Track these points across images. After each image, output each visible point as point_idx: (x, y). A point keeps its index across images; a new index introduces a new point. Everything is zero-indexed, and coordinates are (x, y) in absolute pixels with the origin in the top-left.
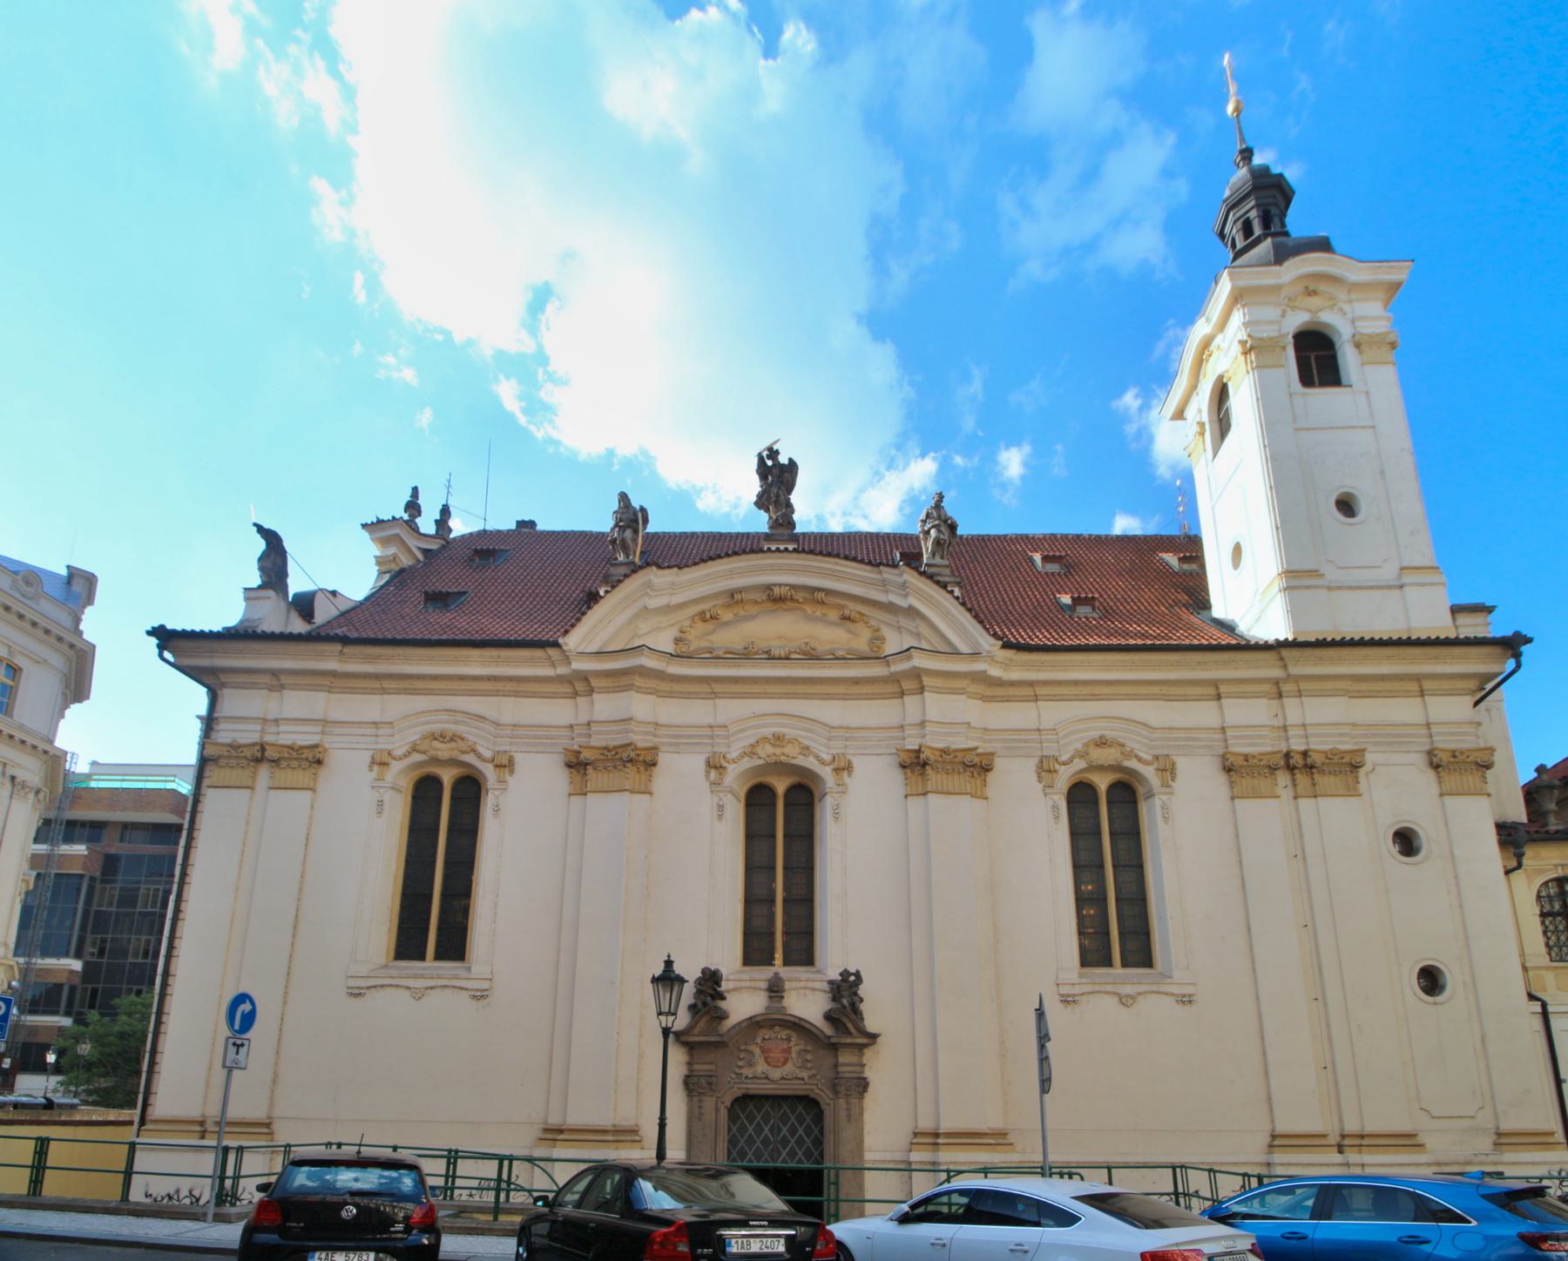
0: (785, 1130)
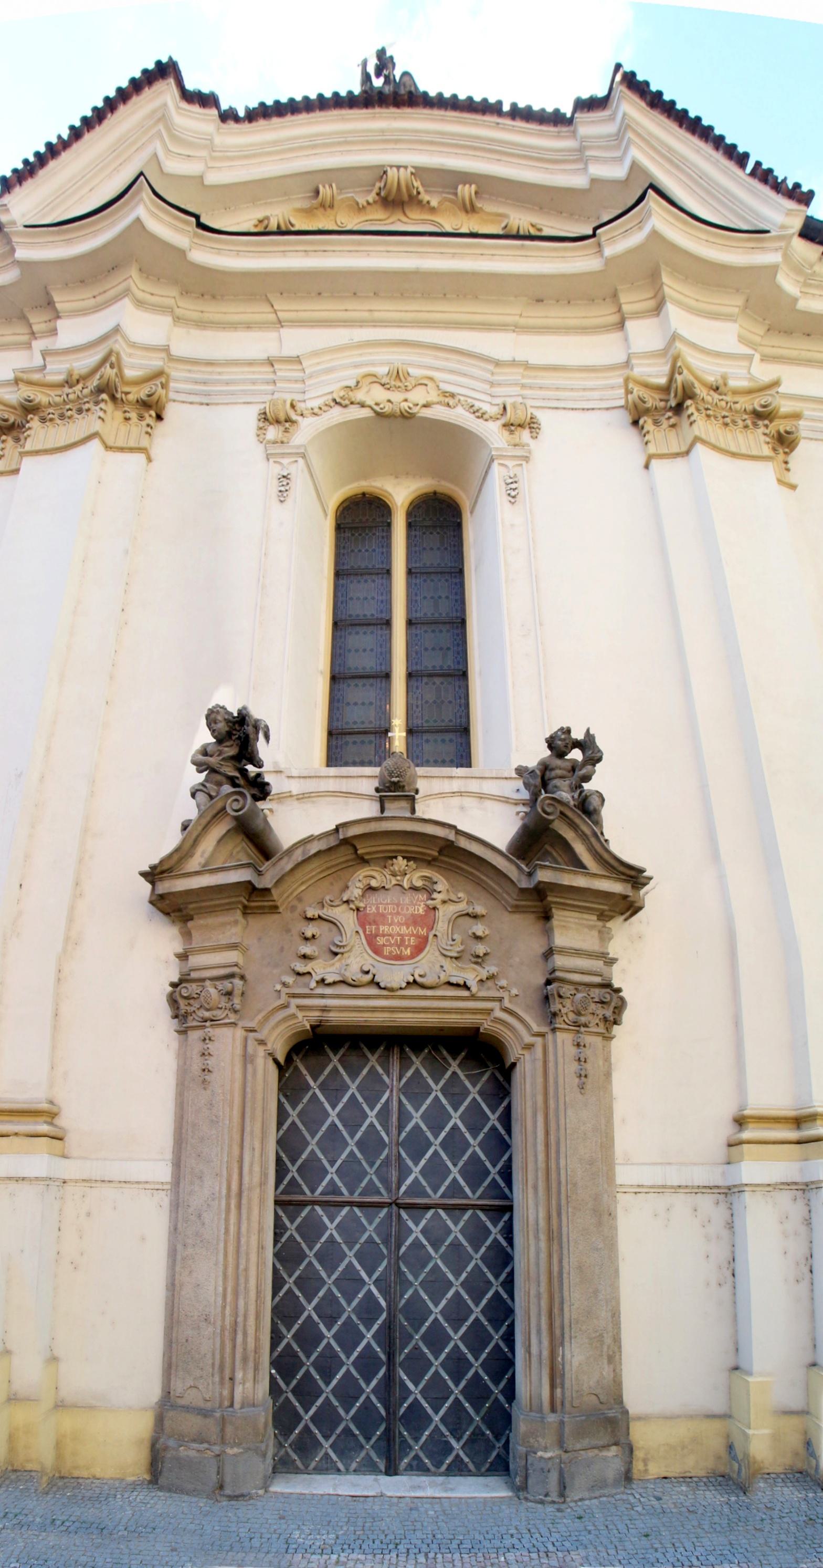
0: (416, 1118)
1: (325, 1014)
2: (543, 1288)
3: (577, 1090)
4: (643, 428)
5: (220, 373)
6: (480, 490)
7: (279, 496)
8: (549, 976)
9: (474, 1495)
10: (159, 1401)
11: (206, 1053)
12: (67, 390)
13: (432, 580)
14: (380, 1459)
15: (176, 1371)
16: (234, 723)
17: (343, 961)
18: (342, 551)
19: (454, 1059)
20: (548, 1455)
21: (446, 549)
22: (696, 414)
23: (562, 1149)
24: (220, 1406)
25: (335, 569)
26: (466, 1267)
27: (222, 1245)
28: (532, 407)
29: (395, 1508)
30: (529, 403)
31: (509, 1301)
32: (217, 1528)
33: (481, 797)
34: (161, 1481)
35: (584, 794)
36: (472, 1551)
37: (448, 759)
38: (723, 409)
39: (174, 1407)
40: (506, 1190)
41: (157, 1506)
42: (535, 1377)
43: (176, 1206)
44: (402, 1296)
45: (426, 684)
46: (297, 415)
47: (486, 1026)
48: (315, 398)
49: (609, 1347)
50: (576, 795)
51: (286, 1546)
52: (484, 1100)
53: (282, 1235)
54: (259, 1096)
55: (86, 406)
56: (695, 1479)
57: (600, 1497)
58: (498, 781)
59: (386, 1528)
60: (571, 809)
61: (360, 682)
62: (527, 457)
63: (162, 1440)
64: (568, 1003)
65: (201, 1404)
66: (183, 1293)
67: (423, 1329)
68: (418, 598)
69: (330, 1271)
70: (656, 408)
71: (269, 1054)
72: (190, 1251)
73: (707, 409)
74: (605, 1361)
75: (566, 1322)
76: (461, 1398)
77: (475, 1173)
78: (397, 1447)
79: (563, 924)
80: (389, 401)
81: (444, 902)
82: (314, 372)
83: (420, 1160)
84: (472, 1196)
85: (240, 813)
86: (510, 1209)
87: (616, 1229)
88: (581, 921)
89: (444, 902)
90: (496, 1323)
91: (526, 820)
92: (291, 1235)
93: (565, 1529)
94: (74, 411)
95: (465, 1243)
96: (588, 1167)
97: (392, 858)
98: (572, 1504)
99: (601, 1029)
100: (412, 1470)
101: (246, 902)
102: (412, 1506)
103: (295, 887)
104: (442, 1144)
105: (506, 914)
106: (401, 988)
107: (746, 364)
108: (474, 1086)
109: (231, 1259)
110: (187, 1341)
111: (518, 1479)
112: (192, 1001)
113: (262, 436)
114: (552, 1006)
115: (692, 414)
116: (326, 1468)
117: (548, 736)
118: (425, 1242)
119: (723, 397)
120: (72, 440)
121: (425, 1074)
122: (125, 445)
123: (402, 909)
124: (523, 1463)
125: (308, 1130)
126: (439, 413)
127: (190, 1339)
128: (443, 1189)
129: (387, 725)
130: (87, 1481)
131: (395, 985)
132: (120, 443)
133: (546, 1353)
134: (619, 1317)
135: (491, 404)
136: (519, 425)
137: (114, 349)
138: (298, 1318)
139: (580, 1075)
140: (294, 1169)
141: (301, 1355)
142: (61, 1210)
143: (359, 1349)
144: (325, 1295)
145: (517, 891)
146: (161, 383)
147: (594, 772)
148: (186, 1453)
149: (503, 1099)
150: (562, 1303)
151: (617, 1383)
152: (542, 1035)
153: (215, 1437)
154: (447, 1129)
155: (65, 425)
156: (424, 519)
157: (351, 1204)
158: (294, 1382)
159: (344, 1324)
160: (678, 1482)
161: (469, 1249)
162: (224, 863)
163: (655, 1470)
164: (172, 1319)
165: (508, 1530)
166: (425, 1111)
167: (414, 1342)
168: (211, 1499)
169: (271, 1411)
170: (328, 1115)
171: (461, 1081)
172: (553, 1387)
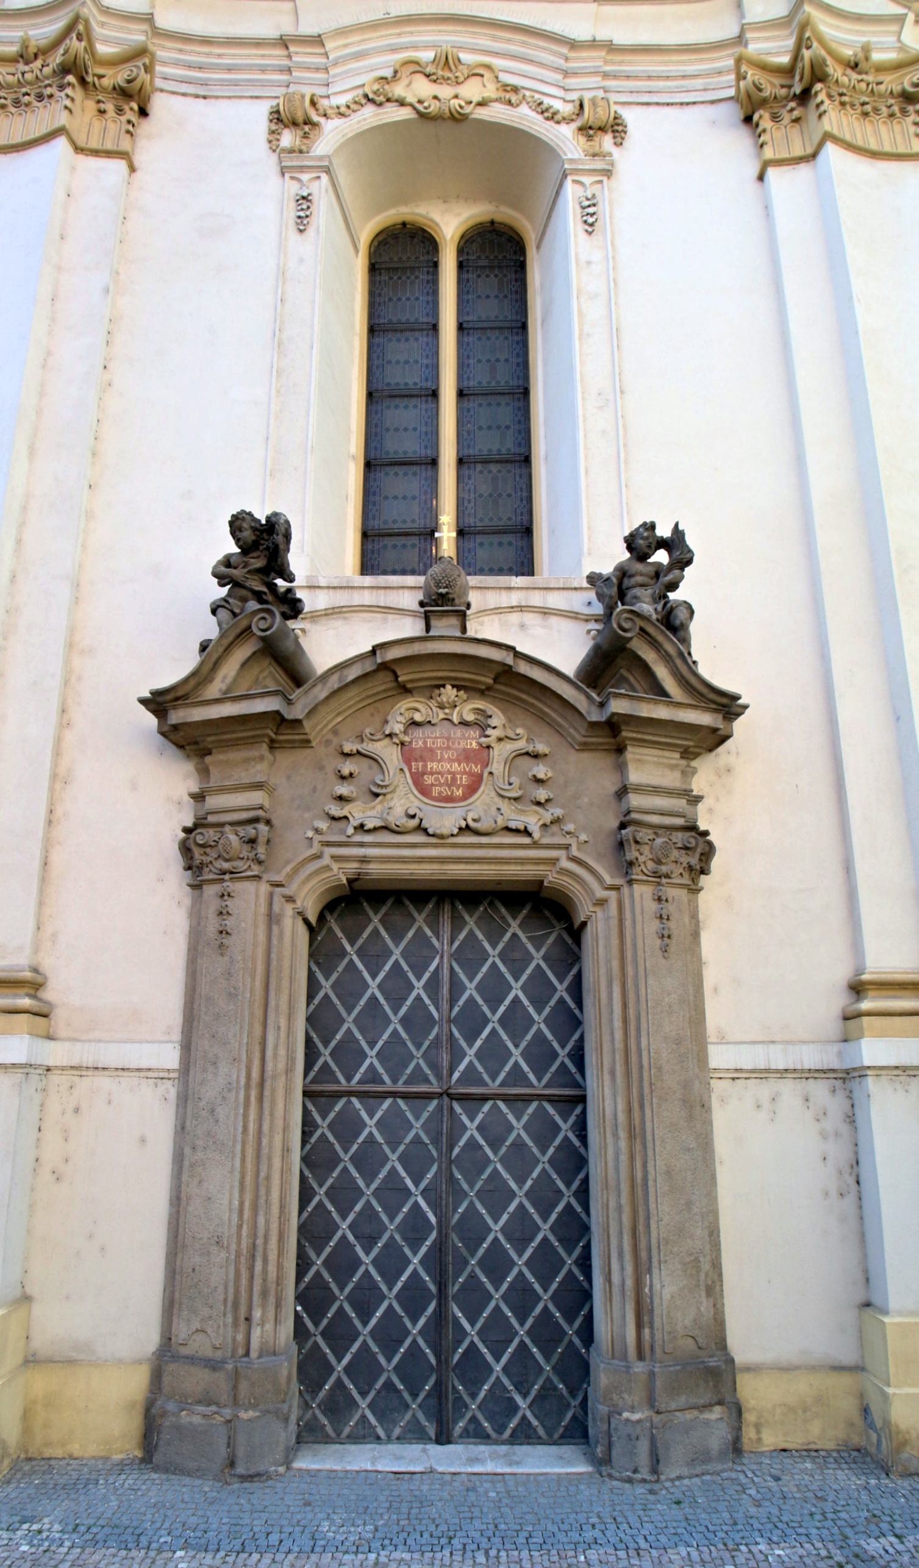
0: (471, 989)
1: (364, 866)
2: (625, 1200)
3: (659, 953)
4: (757, 125)
5: (220, 56)
6: (549, 217)
7: (297, 224)
8: (622, 819)
9: (544, 1470)
10: (158, 1350)
11: (224, 912)
12: (22, 67)
13: (489, 339)
14: (429, 1421)
15: (180, 1310)
16: (262, 532)
17: (385, 804)
18: (377, 299)
19: (514, 918)
20: (636, 1417)
21: (506, 297)
22: (827, 102)
23: (644, 1026)
24: (233, 1356)
25: (369, 323)
26: (532, 1172)
27: (239, 1147)
28: (616, 103)
29: (448, 1488)
30: (613, 97)
31: (583, 1216)
32: (225, 1521)
33: (546, 612)
34: (158, 1458)
35: (669, 605)
36: (544, 1546)
37: (505, 568)
38: (862, 93)
39: (176, 1358)
40: (578, 1077)
41: (150, 1494)
42: (617, 1314)
43: (183, 1099)
44: (455, 1210)
45: (481, 472)
46: (319, 115)
47: (551, 879)
48: (340, 92)
49: (707, 1275)
50: (660, 607)
51: (312, 1543)
52: (550, 967)
53: (311, 1134)
54: (286, 964)
55: (48, 91)
56: (822, 1453)
57: (703, 1474)
58: (565, 593)
59: (437, 1516)
60: (654, 624)
61: (400, 470)
62: (609, 171)
63: (159, 1402)
64: (646, 850)
65: (209, 1353)
66: (190, 1209)
67: (481, 1252)
68: (471, 361)
69: (369, 1179)
70: (775, 97)
71: (299, 913)
72: (200, 1155)
73: (841, 95)
74: (703, 1294)
75: (654, 1241)
76: (527, 1340)
77: (540, 1055)
78: (450, 1406)
79: (639, 757)
80: (435, 98)
81: (500, 740)
82: (339, 58)
83: (475, 1040)
84: (537, 1084)
85: (268, 633)
86: (582, 1099)
87: (711, 1124)
88: (661, 760)
89: (500, 740)
90: (569, 1244)
91: (598, 640)
92: (323, 1134)
93: (659, 1518)
94: (32, 96)
95: (530, 1143)
96: (675, 1047)
97: (438, 687)
98: (668, 1484)
99: (686, 880)
100: (468, 1437)
101: (273, 736)
102: (469, 1485)
103: (328, 719)
104: (502, 1021)
105: (573, 751)
106: (452, 835)
107: (894, 28)
108: (538, 950)
109: (249, 1165)
110: (194, 1270)
111: (599, 1450)
112: (208, 850)
113: (275, 142)
114: (627, 854)
115: (822, 102)
116: (363, 1435)
117: (627, 533)
118: (482, 1142)
119: (864, 77)
120: (32, 137)
121: (480, 936)
122: (100, 147)
123: (453, 743)
124: (606, 1427)
125: (343, 1004)
126: (497, 113)
127: (197, 1268)
128: (502, 1075)
129: (434, 525)
130: (61, 1463)
131: (445, 831)
132: (94, 144)
133: (629, 1283)
134: (719, 1236)
135: (565, 101)
136: (600, 129)
137: (82, 14)
138: (330, 1239)
139: (663, 936)
140: (327, 1052)
141: (333, 1286)
142: (42, 1105)
143: (403, 1278)
144: (363, 1209)
145: (586, 725)
146: (144, 65)
147: (683, 577)
148: (188, 1419)
149: (572, 965)
150: (648, 1218)
151: (719, 1322)
152: (617, 888)
153: (225, 1397)
154: (507, 1002)
155: (20, 114)
156: (479, 257)
157: (394, 1095)
158: (325, 1322)
159: (386, 1246)
160: (800, 1457)
161: (535, 1150)
162: (250, 689)
163: (771, 1439)
164: (176, 1243)
165: (588, 1518)
166: (481, 981)
167: (469, 1269)
168: (219, 1481)
169: (295, 1360)
170: (367, 986)
171: (522, 943)
172: (639, 1326)
